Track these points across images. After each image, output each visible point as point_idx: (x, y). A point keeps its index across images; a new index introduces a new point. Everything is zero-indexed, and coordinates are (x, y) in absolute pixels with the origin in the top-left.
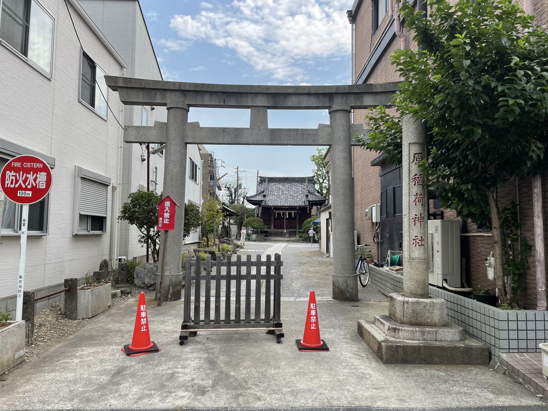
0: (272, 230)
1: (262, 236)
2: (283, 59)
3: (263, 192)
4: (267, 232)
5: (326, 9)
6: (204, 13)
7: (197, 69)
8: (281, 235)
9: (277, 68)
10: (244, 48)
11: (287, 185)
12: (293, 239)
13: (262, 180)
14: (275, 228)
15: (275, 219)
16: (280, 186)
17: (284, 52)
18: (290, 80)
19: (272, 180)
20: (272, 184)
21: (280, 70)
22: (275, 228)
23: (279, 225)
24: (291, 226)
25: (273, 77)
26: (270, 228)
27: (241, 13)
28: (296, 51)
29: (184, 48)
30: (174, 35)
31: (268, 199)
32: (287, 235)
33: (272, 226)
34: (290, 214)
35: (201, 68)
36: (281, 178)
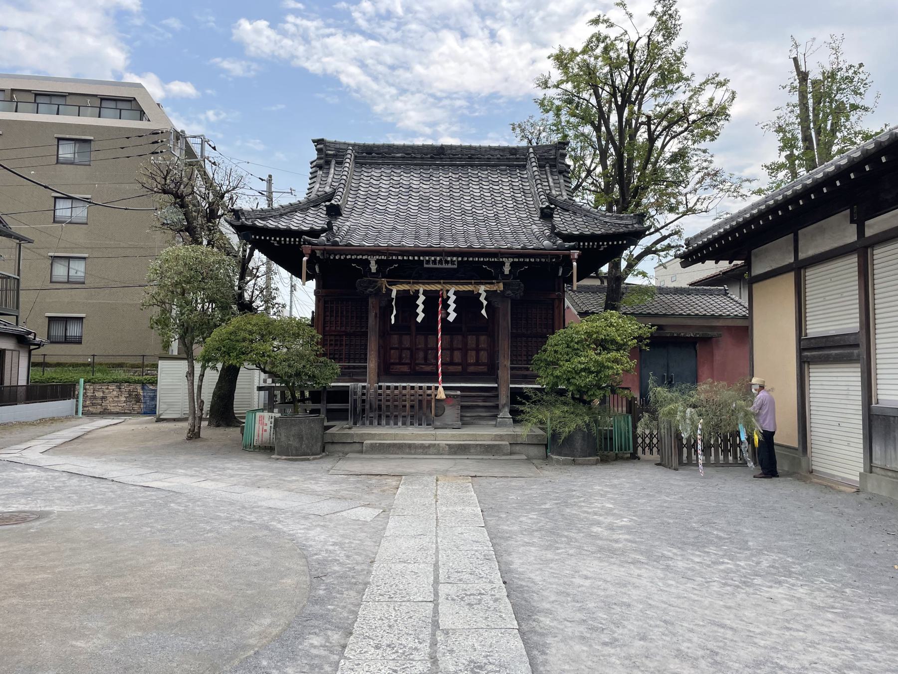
0: (368, 385)
1: (307, 424)
2: (418, 97)
3: (329, 197)
4: (342, 395)
5: (489, 22)
6: (291, 18)
7: (274, 108)
8: (421, 412)
9: (407, 110)
10: (352, 76)
11: (444, 178)
12: (484, 433)
13: (328, 155)
14: (386, 371)
15: (386, 331)
16: (413, 179)
17: (421, 84)
18: (428, 130)
19: (372, 156)
20: (376, 173)
21: (412, 114)
22: (386, 371)
23: (407, 356)
24: (464, 364)
25: (400, 125)
26: (359, 374)
27: (353, 21)
28: (438, 85)
29: (253, 73)
30: (238, 50)
31: (343, 225)
32: (451, 413)
33: (372, 364)
34: (467, 302)
35: (281, 107)
36: (414, 148)
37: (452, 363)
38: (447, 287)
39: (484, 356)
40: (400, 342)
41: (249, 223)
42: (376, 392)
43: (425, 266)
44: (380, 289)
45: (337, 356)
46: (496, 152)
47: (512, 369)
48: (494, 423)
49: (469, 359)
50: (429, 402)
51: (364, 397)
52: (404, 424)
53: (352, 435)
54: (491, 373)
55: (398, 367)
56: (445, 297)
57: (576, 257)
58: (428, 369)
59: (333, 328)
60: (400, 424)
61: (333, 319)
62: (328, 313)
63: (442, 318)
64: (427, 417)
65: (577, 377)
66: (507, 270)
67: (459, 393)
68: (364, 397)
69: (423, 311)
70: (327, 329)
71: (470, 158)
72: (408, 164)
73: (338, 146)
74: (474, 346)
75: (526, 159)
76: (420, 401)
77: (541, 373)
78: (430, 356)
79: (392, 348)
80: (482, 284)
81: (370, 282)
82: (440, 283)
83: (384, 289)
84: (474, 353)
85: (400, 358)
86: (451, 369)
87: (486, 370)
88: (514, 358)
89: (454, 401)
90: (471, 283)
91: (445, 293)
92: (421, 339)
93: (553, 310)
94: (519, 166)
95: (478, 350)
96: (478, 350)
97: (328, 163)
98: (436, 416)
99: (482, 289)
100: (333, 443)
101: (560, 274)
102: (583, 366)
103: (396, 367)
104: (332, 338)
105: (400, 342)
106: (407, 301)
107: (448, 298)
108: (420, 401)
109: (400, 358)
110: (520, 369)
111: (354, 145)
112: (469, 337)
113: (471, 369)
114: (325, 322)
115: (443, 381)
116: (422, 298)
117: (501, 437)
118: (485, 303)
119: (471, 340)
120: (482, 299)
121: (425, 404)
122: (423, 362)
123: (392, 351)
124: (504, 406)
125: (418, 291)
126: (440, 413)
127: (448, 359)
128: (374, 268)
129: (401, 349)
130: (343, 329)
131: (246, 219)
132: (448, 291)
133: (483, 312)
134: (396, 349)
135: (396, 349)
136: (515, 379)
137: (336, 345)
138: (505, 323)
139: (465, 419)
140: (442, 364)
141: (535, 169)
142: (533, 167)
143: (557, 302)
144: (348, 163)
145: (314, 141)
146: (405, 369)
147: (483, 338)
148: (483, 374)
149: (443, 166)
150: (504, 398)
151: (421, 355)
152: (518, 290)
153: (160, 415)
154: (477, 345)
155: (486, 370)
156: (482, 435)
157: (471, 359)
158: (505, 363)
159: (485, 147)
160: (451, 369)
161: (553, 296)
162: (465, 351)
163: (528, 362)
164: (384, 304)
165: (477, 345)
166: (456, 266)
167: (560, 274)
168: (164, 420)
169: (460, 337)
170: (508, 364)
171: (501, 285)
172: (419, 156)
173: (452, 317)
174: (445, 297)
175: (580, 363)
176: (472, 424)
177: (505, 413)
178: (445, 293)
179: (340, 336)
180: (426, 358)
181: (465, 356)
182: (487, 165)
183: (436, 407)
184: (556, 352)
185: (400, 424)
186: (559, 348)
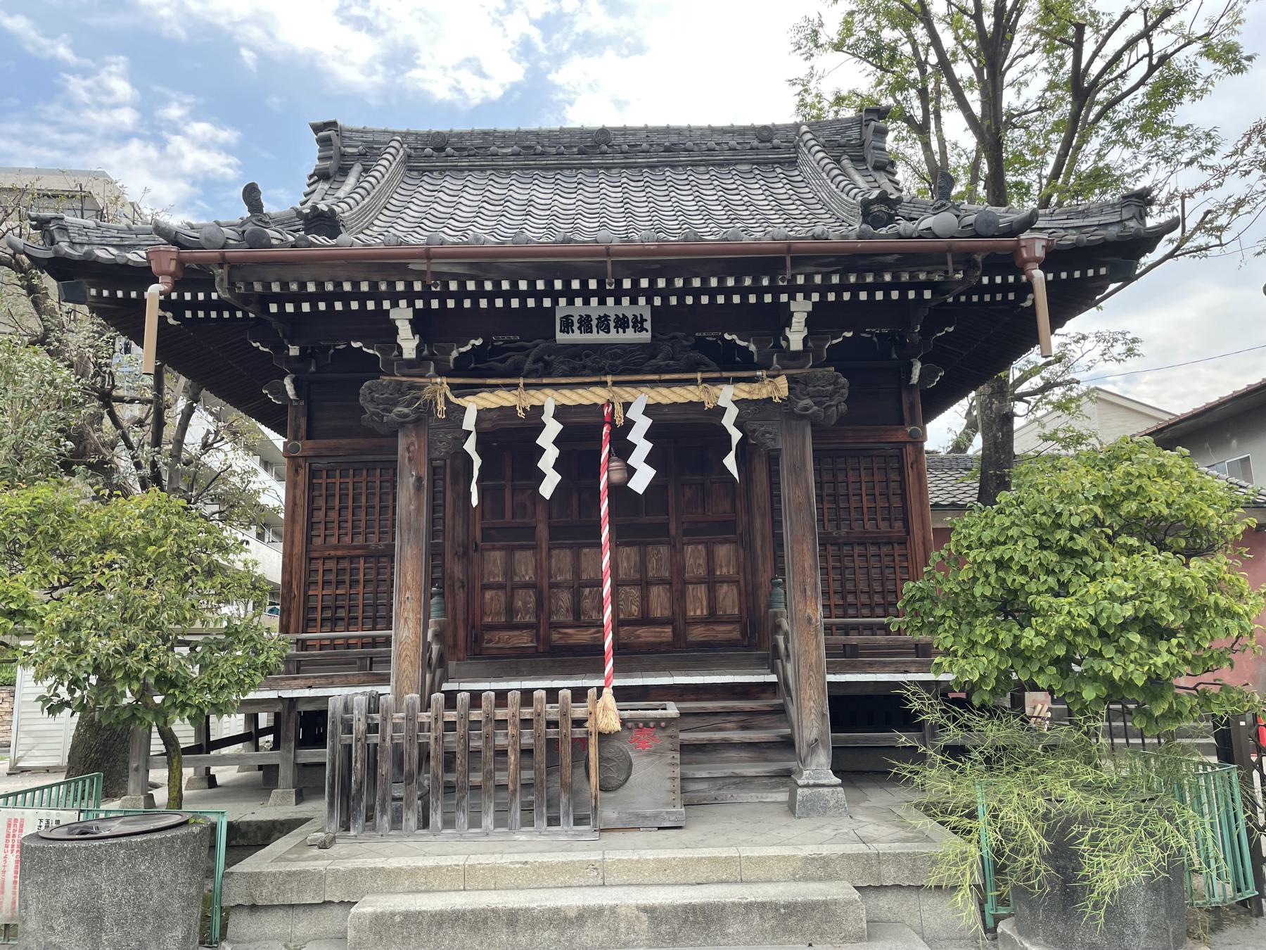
14: (466, 641)
22: (466, 641)
32: (652, 776)
33: (408, 630)
34: (686, 439)
37: (645, 620)
38: (626, 393)
39: (729, 598)
40: (509, 570)
41: (76, 253)
42: (410, 718)
43: (561, 337)
44: (430, 406)
45: (341, 613)
46: (727, 138)
47: (828, 629)
48: (782, 796)
49: (690, 606)
50: (580, 745)
51: (375, 738)
52: (499, 823)
53: (319, 879)
54: (755, 637)
55: (505, 635)
56: (620, 421)
57: (1039, 252)
58: (582, 636)
59: (334, 540)
60: (488, 821)
61: (333, 515)
62: (321, 502)
63: (611, 486)
64: (573, 792)
65: (1109, 652)
66: (796, 337)
67: (672, 710)
68: (375, 738)
69: (542, 451)
70: (318, 541)
71: (667, 150)
72: (528, 167)
73: (370, 138)
74: (702, 572)
75: (796, 147)
76: (552, 745)
77: (944, 639)
78: (587, 603)
79: (486, 587)
80: (726, 381)
81: (399, 388)
82: (603, 384)
83: (441, 407)
84: (702, 591)
85: (510, 610)
86: (646, 634)
87: (736, 635)
88: (840, 598)
89: (661, 739)
90: (693, 382)
91: (619, 410)
92: (562, 559)
93: (901, 471)
94: (780, 163)
95: (711, 582)
96: (711, 582)
97: (344, 171)
98: (604, 788)
99: (726, 395)
100: (254, 908)
101: (915, 378)
102: (1128, 610)
103: (497, 635)
104: (331, 565)
105: (509, 570)
106: (510, 441)
107: (629, 424)
108: (552, 745)
109: (510, 610)
110: (858, 629)
111: (406, 135)
112: (689, 549)
113: (697, 633)
114: (311, 526)
115: (619, 669)
116: (552, 428)
117: (821, 868)
118: (736, 435)
119: (694, 558)
120: (728, 421)
121: (566, 750)
122: (570, 618)
123: (488, 595)
124: (813, 747)
125: (539, 410)
126: (616, 777)
127: (635, 609)
128: (408, 344)
129: (510, 587)
130: (359, 540)
131: (73, 244)
132: (627, 406)
133: (730, 462)
134: (499, 587)
135: (499, 587)
136: (843, 656)
137: (339, 583)
138: (800, 488)
139: (695, 786)
140: (618, 623)
141: (821, 155)
142: (814, 156)
143: (910, 449)
144: (386, 166)
145: (317, 128)
146: (524, 640)
147: (724, 552)
148: (730, 645)
149: (608, 168)
150: (811, 719)
151: (565, 599)
152: (831, 396)
153: (20, 759)
154: (711, 570)
155: (736, 635)
156: (762, 860)
157: (696, 608)
158: (804, 618)
159: (700, 129)
160: (646, 634)
161: (900, 437)
162: (678, 585)
163: (888, 607)
164: (442, 448)
165: (711, 570)
166: (646, 336)
167: (915, 378)
168: (24, 770)
169: (664, 550)
170: (817, 614)
171: (782, 382)
172: (553, 150)
173: (642, 480)
174: (620, 421)
175: (1111, 596)
176: (715, 802)
177: (818, 769)
178: (619, 410)
179: (352, 559)
180: (577, 610)
181: (679, 598)
182: (707, 164)
183: (602, 759)
184: (1001, 564)
185: (488, 821)
186: (1017, 553)
